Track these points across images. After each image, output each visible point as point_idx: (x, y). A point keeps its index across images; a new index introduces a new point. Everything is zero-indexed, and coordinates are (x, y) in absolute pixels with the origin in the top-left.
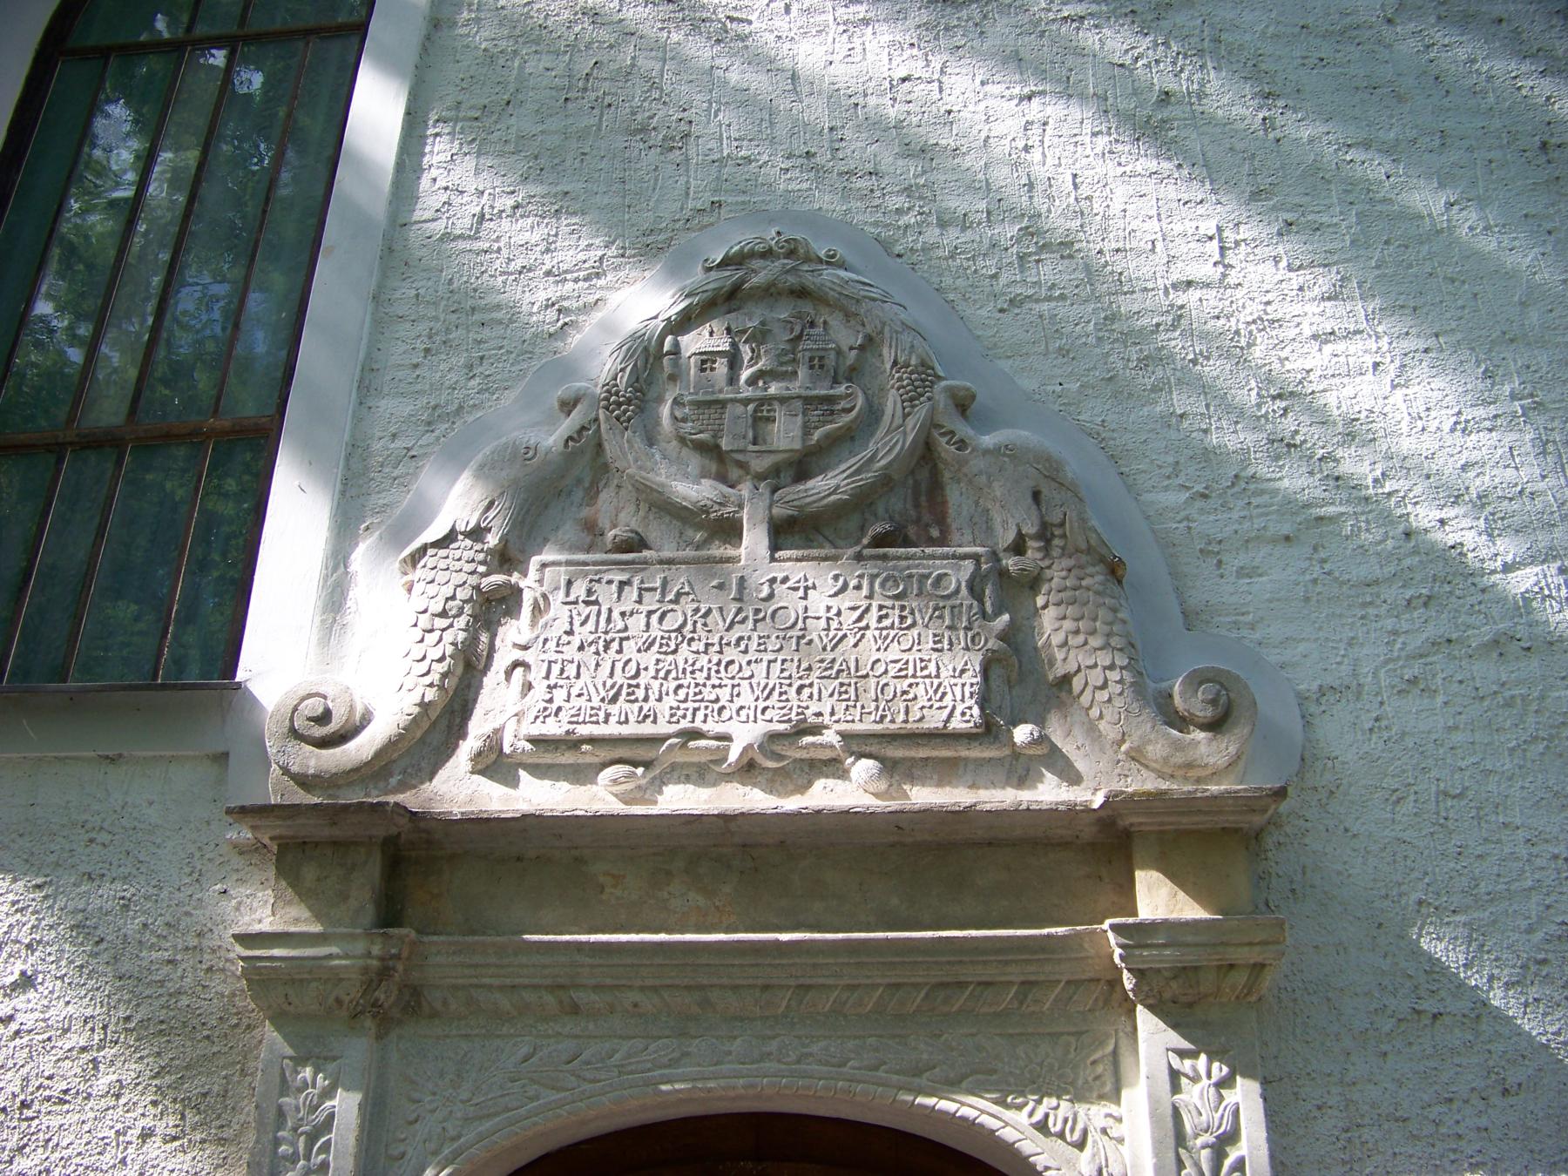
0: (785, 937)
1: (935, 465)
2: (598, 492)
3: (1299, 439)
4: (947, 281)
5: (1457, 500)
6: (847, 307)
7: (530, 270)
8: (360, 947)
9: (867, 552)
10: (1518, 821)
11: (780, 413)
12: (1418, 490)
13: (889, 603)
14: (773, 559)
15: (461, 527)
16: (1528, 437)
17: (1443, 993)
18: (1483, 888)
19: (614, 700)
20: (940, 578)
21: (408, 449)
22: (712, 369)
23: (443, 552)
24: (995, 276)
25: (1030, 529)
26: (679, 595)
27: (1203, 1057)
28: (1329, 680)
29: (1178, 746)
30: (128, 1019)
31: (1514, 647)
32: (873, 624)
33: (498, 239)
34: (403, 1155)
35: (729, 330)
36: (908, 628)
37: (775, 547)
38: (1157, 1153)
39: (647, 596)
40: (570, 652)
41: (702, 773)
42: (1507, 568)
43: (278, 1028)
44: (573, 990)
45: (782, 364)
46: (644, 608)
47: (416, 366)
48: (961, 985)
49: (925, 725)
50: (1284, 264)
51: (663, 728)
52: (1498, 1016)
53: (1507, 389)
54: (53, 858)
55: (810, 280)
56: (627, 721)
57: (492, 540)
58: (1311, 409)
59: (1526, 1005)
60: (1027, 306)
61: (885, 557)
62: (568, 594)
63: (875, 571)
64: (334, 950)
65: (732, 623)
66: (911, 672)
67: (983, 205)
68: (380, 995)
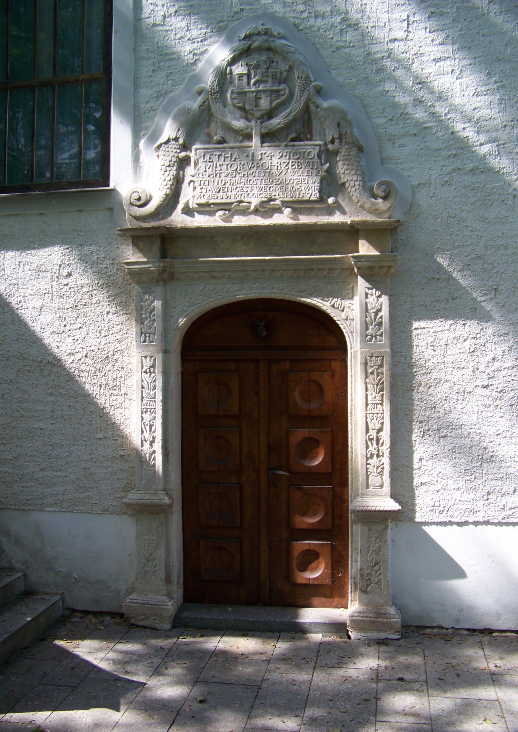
0: (267, 258)
1: (310, 113)
2: (210, 123)
3: (424, 98)
4: (317, 40)
5: (470, 121)
6: (284, 54)
7: (183, 38)
8: (157, 264)
9: (289, 144)
10: (469, 225)
11: (263, 96)
12: (458, 117)
13: (294, 161)
14: (262, 147)
15: (171, 137)
16: (497, 97)
17: (441, 273)
18: (456, 244)
19: (219, 192)
20: (309, 152)
21: (152, 107)
22: (242, 80)
23: (167, 146)
24: (332, 38)
25: (336, 136)
26: (235, 159)
27: (374, 290)
28: (422, 181)
29: (373, 204)
30: (98, 283)
31: (478, 171)
32: (290, 168)
33: (171, 26)
34: (173, 316)
35: (247, 64)
36: (300, 169)
37: (262, 142)
38: (361, 314)
39: (226, 159)
40: (206, 178)
41: (244, 212)
42: (481, 145)
43: (138, 285)
44: (215, 272)
45: (263, 77)
46: (226, 163)
47: (151, 76)
48: (313, 270)
49: (304, 199)
50: (428, 30)
51: (233, 200)
52: (455, 280)
53: (494, 79)
54: (69, 240)
55: (272, 45)
56: (223, 198)
57: (181, 141)
58: (428, 88)
59: (462, 276)
60: (342, 50)
61: (294, 146)
62: (204, 159)
63: (291, 150)
64: (151, 265)
65: (251, 168)
66: (300, 182)
67: (329, 9)
68: (164, 276)
